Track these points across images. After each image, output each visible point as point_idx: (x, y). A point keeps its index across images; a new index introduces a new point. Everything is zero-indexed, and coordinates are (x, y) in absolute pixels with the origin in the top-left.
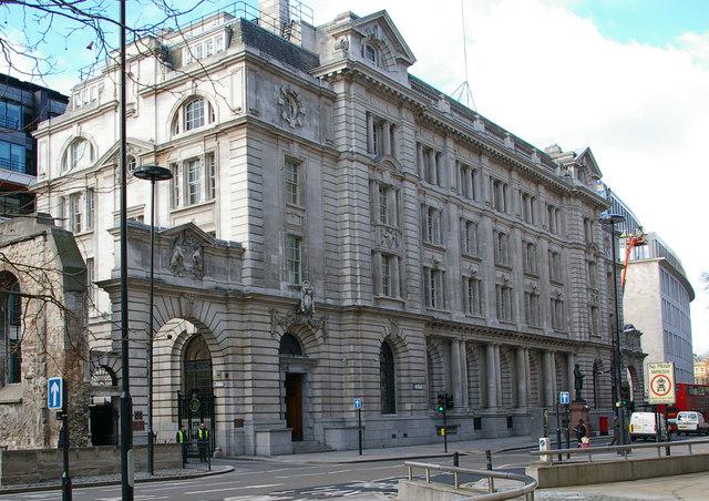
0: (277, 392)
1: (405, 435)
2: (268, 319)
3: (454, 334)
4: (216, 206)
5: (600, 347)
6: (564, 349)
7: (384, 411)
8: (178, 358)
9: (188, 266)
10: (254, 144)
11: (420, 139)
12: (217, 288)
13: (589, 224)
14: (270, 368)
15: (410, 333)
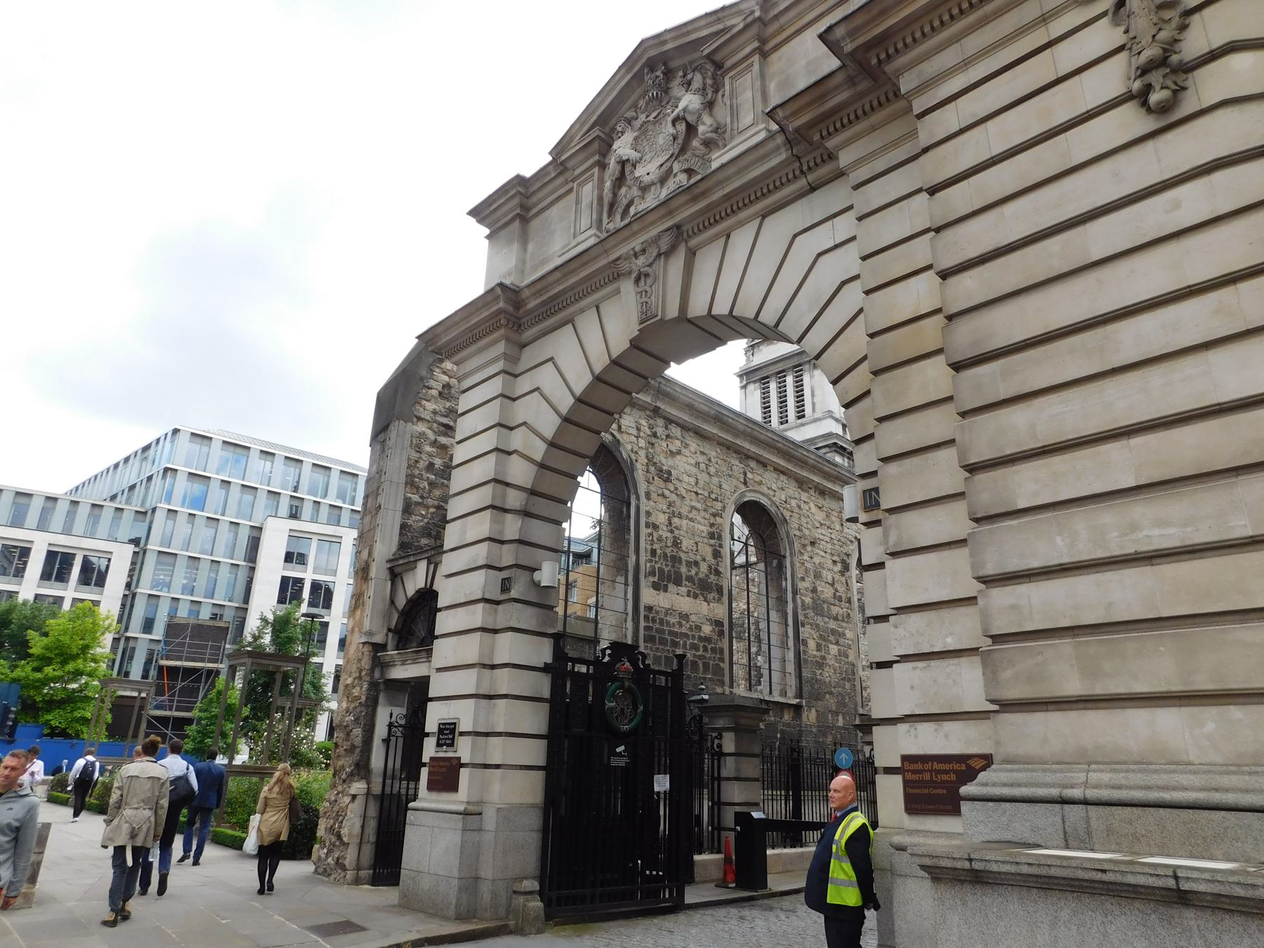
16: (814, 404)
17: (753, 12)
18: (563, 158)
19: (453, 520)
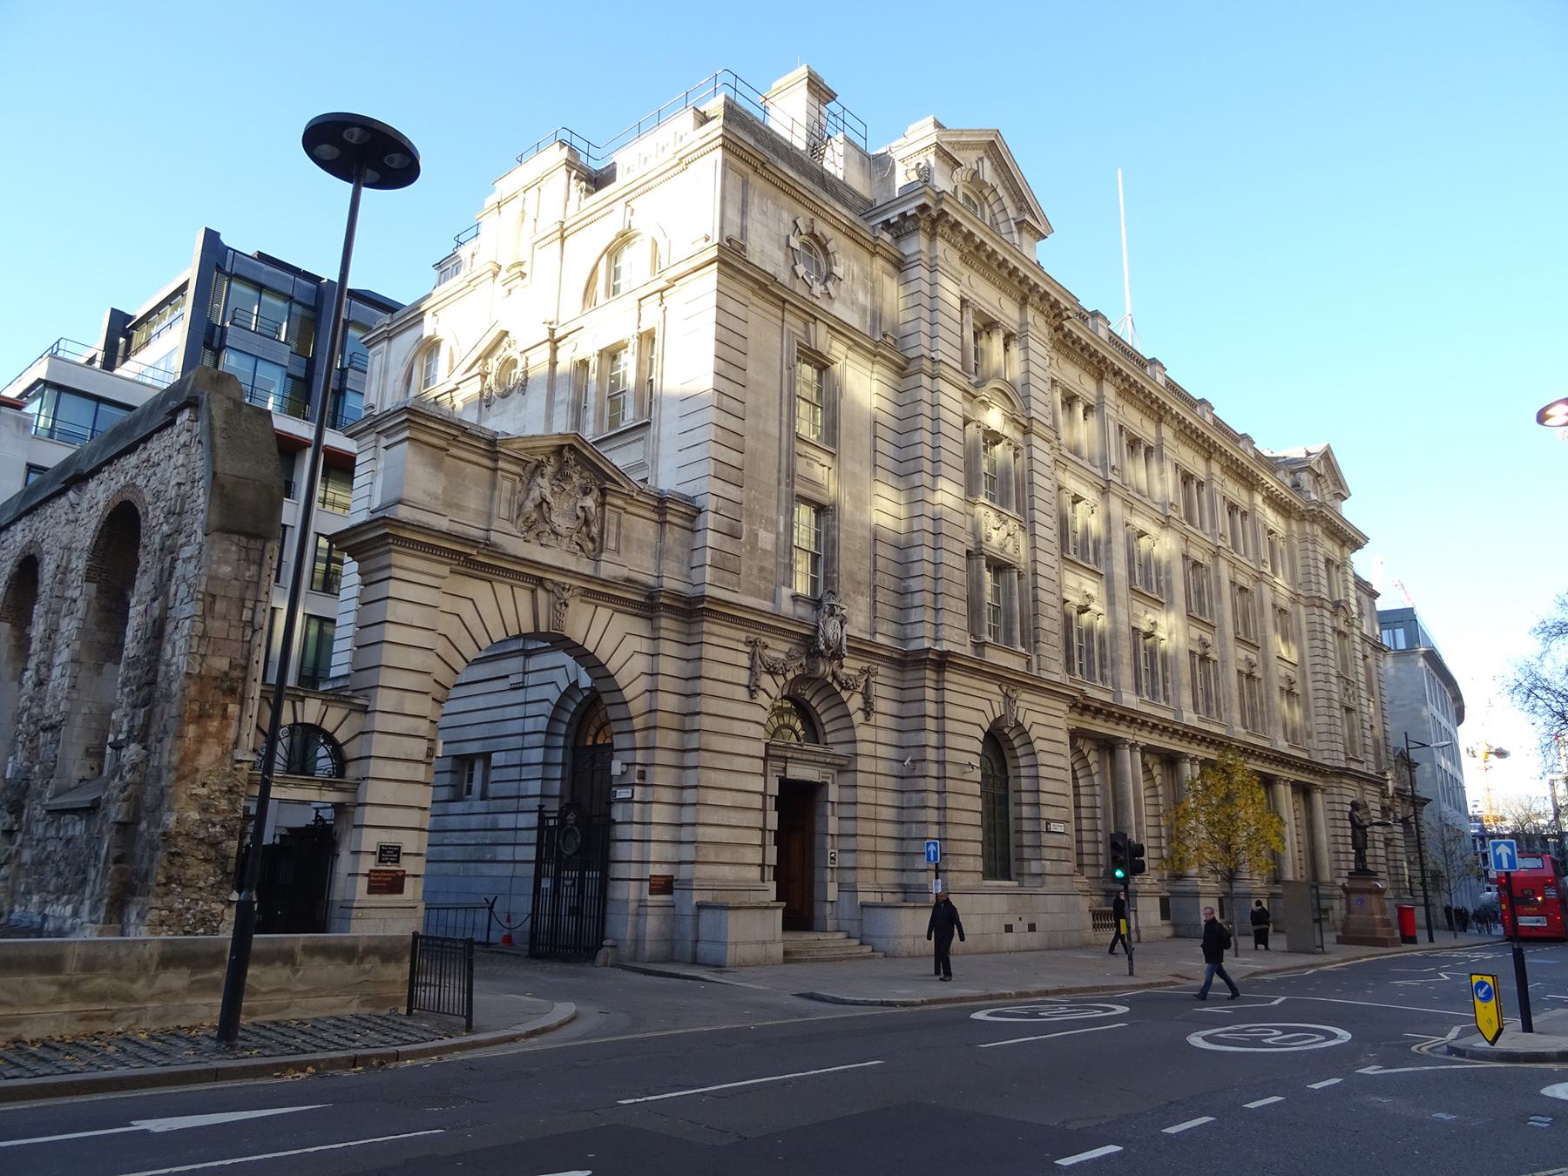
0: (754, 819)
1: (1032, 928)
2: (744, 660)
3: (1121, 731)
4: (653, 429)
5: (1363, 779)
6: (1304, 778)
7: (989, 874)
8: (561, 741)
9: (562, 522)
10: (732, 306)
11: (1058, 375)
12: (628, 580)
13: (1333, 570)
14: (740, 763)
15: (1042, 719)
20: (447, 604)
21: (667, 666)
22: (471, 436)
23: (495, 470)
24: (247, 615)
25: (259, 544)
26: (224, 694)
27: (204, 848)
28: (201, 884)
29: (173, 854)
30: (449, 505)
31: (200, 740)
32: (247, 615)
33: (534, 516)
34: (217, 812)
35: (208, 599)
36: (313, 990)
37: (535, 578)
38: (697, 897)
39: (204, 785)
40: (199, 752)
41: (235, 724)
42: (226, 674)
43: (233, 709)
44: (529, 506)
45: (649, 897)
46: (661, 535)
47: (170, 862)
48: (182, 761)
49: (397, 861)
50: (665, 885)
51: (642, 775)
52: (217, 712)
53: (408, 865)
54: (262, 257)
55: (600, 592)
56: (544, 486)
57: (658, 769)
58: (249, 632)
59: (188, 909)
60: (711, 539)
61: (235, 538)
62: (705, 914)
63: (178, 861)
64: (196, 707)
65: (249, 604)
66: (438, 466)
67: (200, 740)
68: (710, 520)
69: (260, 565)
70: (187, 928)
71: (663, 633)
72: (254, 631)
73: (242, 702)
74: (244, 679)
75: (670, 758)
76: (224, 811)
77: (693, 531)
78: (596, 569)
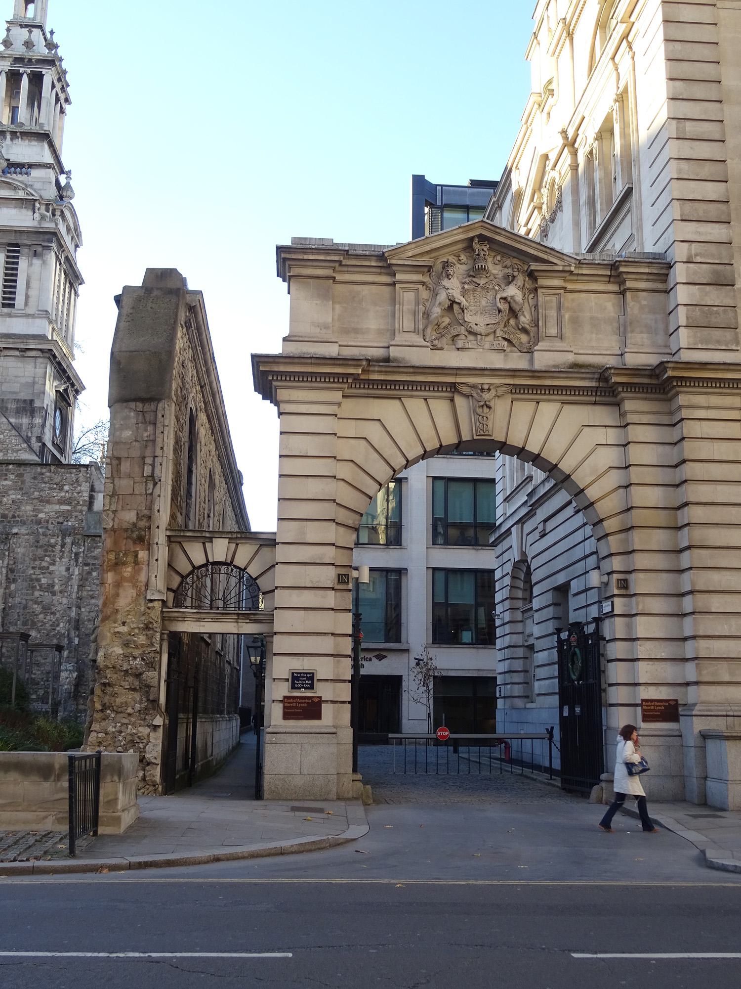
9: (477, 319)
12: (575, 365)
16: (27, 297)
17: (570, 266)
18: (394, 262)
19: (536, 583)
20: (349, 428)
21: (640, 454)
22: (357, 256)
23: (393, 284)
24: (148, 470)
25: (153, 406)
26: (134, 543)
27: (130, 679)
28: (130, 710)
29: (104, 684)
30: (346, 331)
31: (118, 585)
32: (148, 470)
33: (447, 320)
34: (137, 647)
35: (115, 462)
36: (10, 804)
37: (447, 385)
38: (699, 725)
39: (124, 624)
40: (117, 595)
41: (145, 567)
42: (134, 525)
43: (142, 555)
44: (437, 311)
45: (643, 725)
46: (623, 307)
47: (103, 691)
48: (105, 604)
49: (312, 687)
50: (668, 711)
51: (624, 584)
52: (130, 559)
53: (323, 691)
54: (475, 184)
55: (533, 386)
56: (453, 286)
57: (641, 575)
58: (150, 485)
59: (121, 732)
60: (682, 294)
61: (132, 405)
62: (711, 744)
63: (109, 690)
64: (112, 556)
65: (149, 461)
66: (325, 296)
67: (118, 585)
68: (680, 273)
69: (155, 424)
70: (120, 749)
71: (630, 418)
72: (155, 484)
73: (149, 548)
74: (149, 528)
75: (659, 561)
76: (142, 646)
77: (667, 292)
78: (531, 361)
